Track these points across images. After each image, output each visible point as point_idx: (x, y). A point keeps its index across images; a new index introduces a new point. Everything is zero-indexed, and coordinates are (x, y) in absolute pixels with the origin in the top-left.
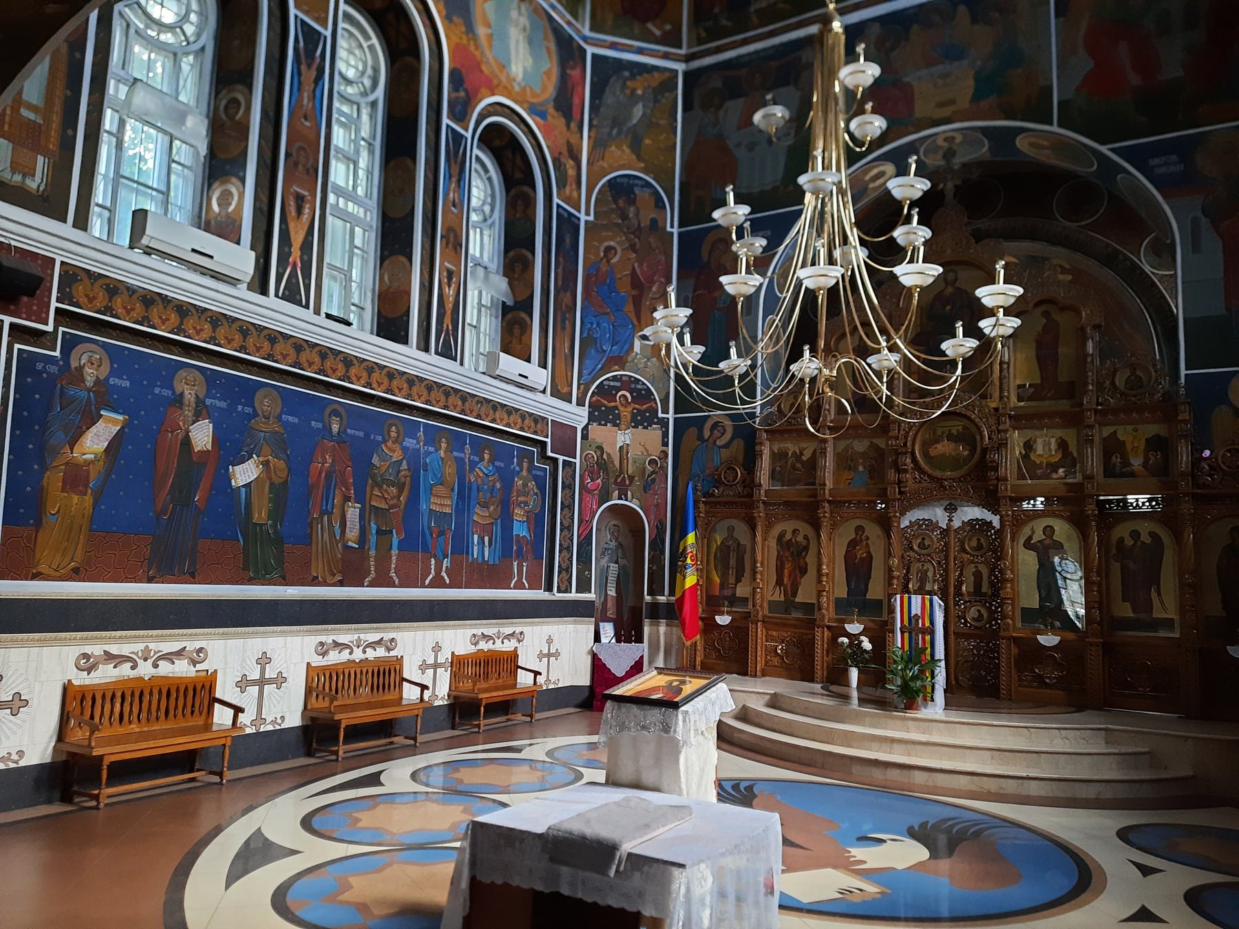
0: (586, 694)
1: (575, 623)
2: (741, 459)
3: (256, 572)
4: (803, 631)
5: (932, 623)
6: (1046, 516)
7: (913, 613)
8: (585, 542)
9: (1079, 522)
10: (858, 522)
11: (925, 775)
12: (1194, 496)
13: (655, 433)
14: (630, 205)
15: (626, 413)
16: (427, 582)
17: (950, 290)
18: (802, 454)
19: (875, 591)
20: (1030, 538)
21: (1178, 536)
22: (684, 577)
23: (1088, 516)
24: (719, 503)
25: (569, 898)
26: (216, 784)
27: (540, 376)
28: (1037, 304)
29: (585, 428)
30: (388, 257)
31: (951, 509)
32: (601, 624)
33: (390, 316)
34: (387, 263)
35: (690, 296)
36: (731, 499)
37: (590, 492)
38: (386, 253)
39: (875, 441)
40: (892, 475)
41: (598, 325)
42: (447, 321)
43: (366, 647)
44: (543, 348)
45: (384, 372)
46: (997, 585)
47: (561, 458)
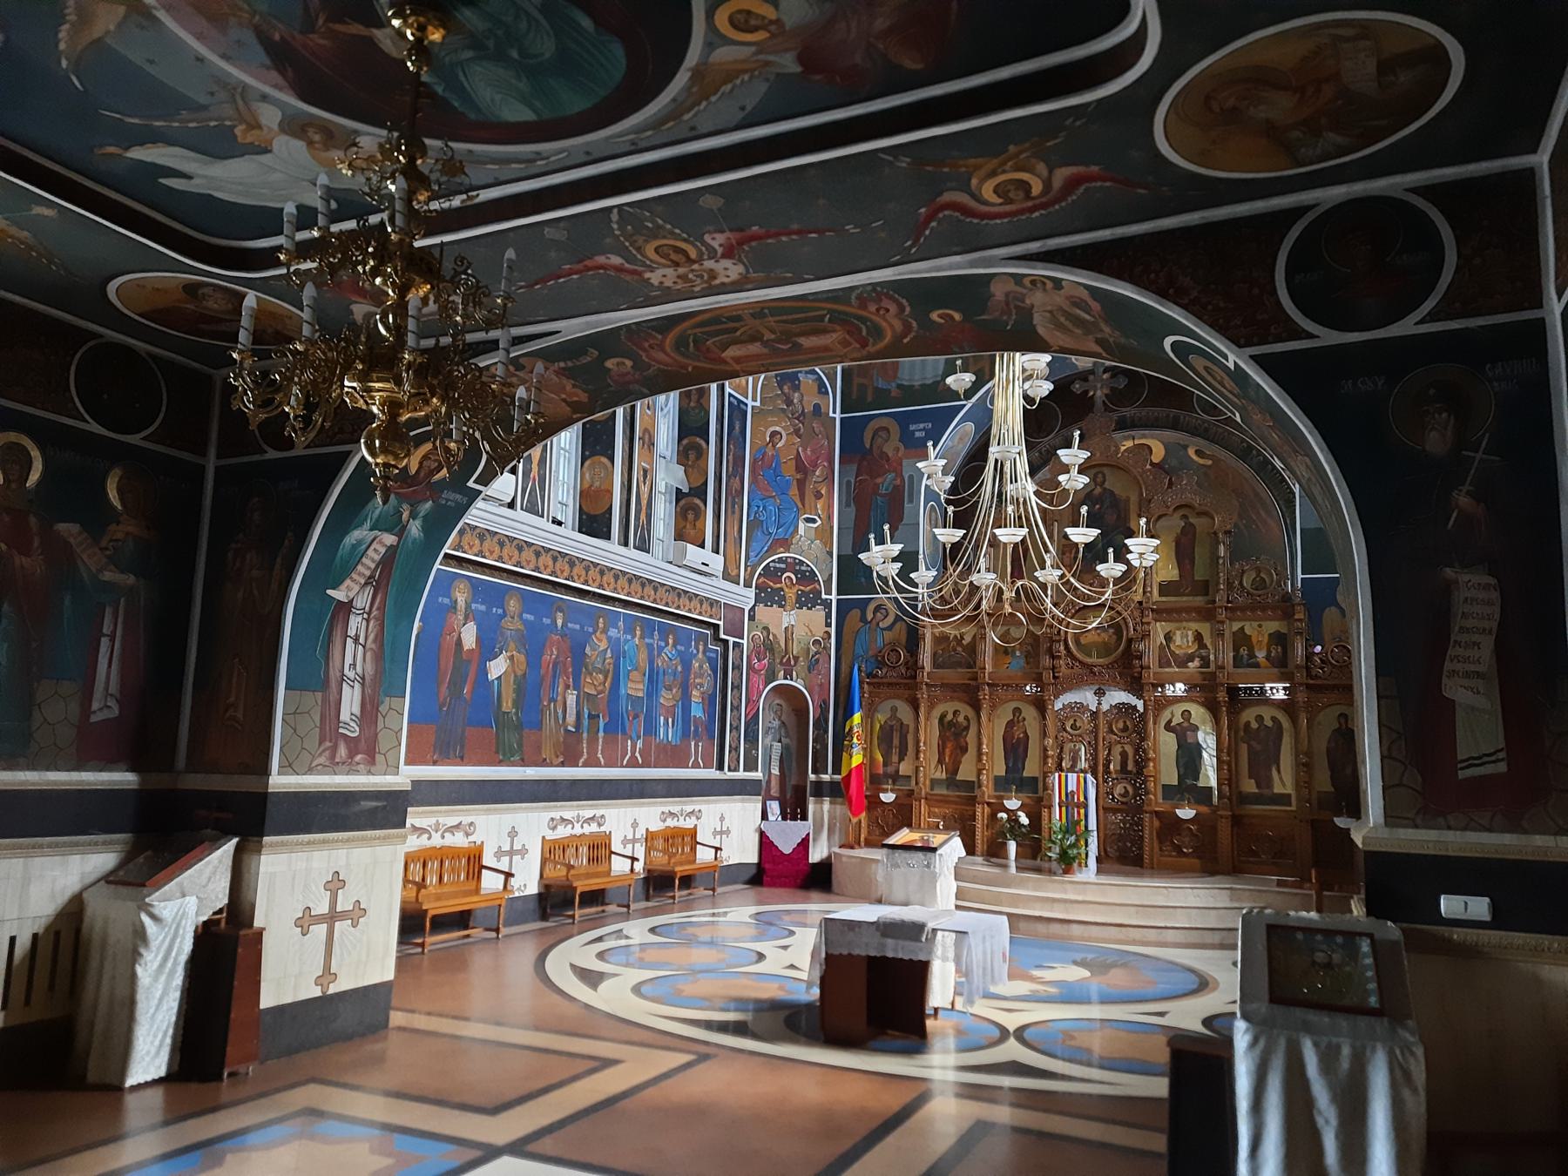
0: (753, 871)
1: (743, 801)
2: (904, 640)
3: (504, 755)
4: (963, 807)
5: (1086, 798)
6: (1188, 701)
7: (1070, 789)
8: (752, 722)
9: (1212, 707)
10: (1014, 705)
11: (1082, 927)
12: (1308, 686)
13: (818, 613)
14: (794, 392)
15: (791, 594)
16: (625, 762)
17: (1098, 490)
18: (962, 638)
19: (1031, 769)
20: (1170, 721)
21: (1294, 720)
22: (851, 756)
23: (1219, 702)
24: (883, 684)
25: (893, 958)
26: (569, 924)
27: (717, 563)
28: (1175, 509)
29: (752, 609)
30: (589, 457)
31: (1100, 693)
32: (768, 803)
33: (592, 513)
34: (587, 463)
35: (853, 481)
36: (894, 680)
37: (757, 672)
38: (587, 453)
39: (1240, 1026)
40: (1046, 661)
41: (764, 508)
42: (643, 516)
43: (444, 832)
44: (716, 534)
45: (567, 559)
46: (1141, 764)
47: (731, 639)
